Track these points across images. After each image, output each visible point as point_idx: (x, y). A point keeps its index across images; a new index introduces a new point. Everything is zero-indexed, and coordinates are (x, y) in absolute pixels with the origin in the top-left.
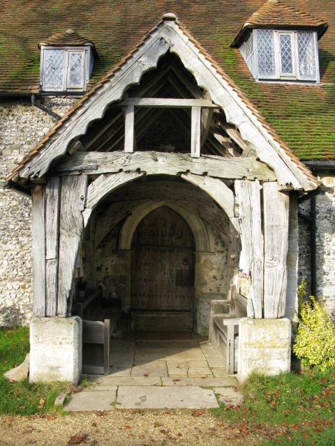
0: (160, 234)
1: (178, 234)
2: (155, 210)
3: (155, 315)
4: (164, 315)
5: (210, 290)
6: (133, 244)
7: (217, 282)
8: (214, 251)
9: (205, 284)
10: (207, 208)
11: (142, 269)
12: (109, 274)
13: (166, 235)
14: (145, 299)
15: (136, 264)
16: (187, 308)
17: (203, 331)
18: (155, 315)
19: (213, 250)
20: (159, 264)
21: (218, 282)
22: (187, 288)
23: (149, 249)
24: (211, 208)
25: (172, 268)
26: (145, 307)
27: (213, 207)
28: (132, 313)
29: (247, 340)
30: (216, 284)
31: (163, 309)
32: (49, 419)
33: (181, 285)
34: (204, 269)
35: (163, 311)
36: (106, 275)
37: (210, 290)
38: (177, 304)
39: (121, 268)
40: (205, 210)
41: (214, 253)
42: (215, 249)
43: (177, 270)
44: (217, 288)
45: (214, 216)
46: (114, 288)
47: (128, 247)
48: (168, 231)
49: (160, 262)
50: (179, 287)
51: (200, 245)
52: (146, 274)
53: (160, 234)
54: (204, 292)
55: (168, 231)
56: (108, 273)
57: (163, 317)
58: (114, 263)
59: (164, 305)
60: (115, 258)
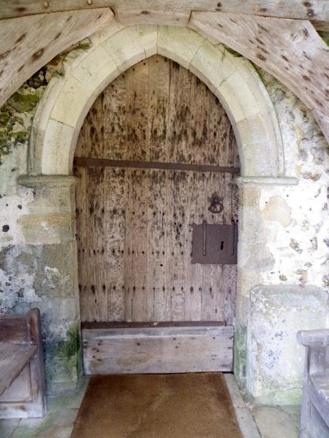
0: (149, 135)
1: (194, 134)
2: (230, 412)
3: (141, 336)
4: (164, 334)
5: (282, 278)
6: (78, 163)
7: (298, 256)
8: (294, 175)
9: (269, 262)
10: (287, 36)
11: (106, 226)
12: (13, 242)
13: (163, 137)
14: (117, 298)
15: (85, 215)
16: (218, 317)
17: (267, 391)
18: (141, 336)
19: (291, 172)
20: (150, 211)
21: (305, 257)
22: (219, 269)
23: (122, 173)
24: (300, 38)
25: (180, 220)
26: (116, 317)
27: (306, 33)
28: (86, 332)
29: (173, 220)
30: (297, 262)
31: (162, 319)
32: (146, 272)
33: (202, 263)
34: (266, 225)
35: (162, 324)
36: (6, 244)
37: (282, 278)
38: (195, 307)
39: (44, 224)
40: (281, 44)
41: (293, 181)
42: (298, 168)
43: (193, 225)
44: (300, 272)
45: (307, 65)
46: (29, 279)
47: (64, 167)
48: (169, 125)
49: (152, 206)
50: (199, 265)
51: (254, 158)
52: (117, 236)
53: (149, 135)
54: (266, 282)
55: (169, 125)
56: (10, 239)
57: (161, 341)
58: (25, 211)
59: (162, 315)
60: (26, 197)
